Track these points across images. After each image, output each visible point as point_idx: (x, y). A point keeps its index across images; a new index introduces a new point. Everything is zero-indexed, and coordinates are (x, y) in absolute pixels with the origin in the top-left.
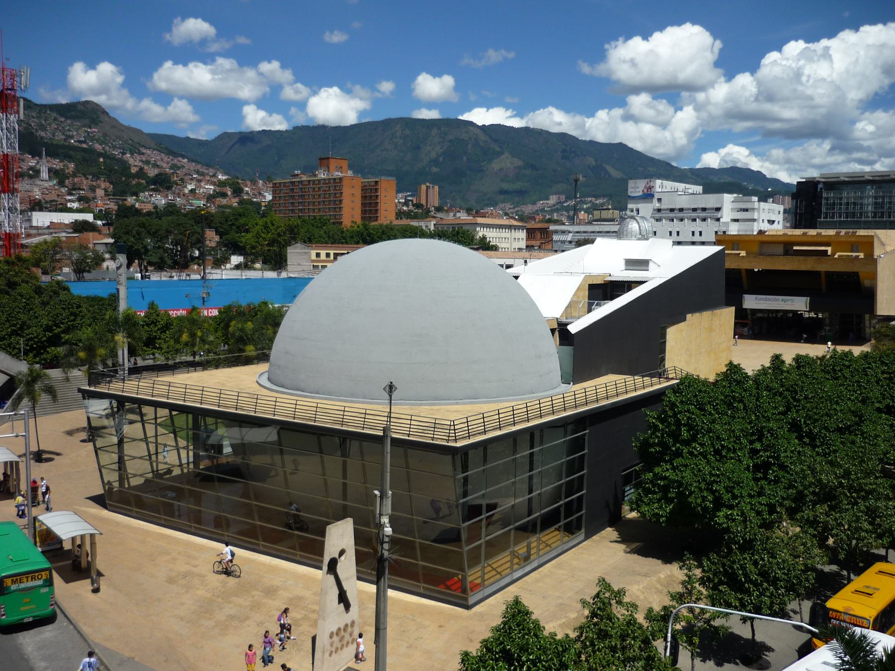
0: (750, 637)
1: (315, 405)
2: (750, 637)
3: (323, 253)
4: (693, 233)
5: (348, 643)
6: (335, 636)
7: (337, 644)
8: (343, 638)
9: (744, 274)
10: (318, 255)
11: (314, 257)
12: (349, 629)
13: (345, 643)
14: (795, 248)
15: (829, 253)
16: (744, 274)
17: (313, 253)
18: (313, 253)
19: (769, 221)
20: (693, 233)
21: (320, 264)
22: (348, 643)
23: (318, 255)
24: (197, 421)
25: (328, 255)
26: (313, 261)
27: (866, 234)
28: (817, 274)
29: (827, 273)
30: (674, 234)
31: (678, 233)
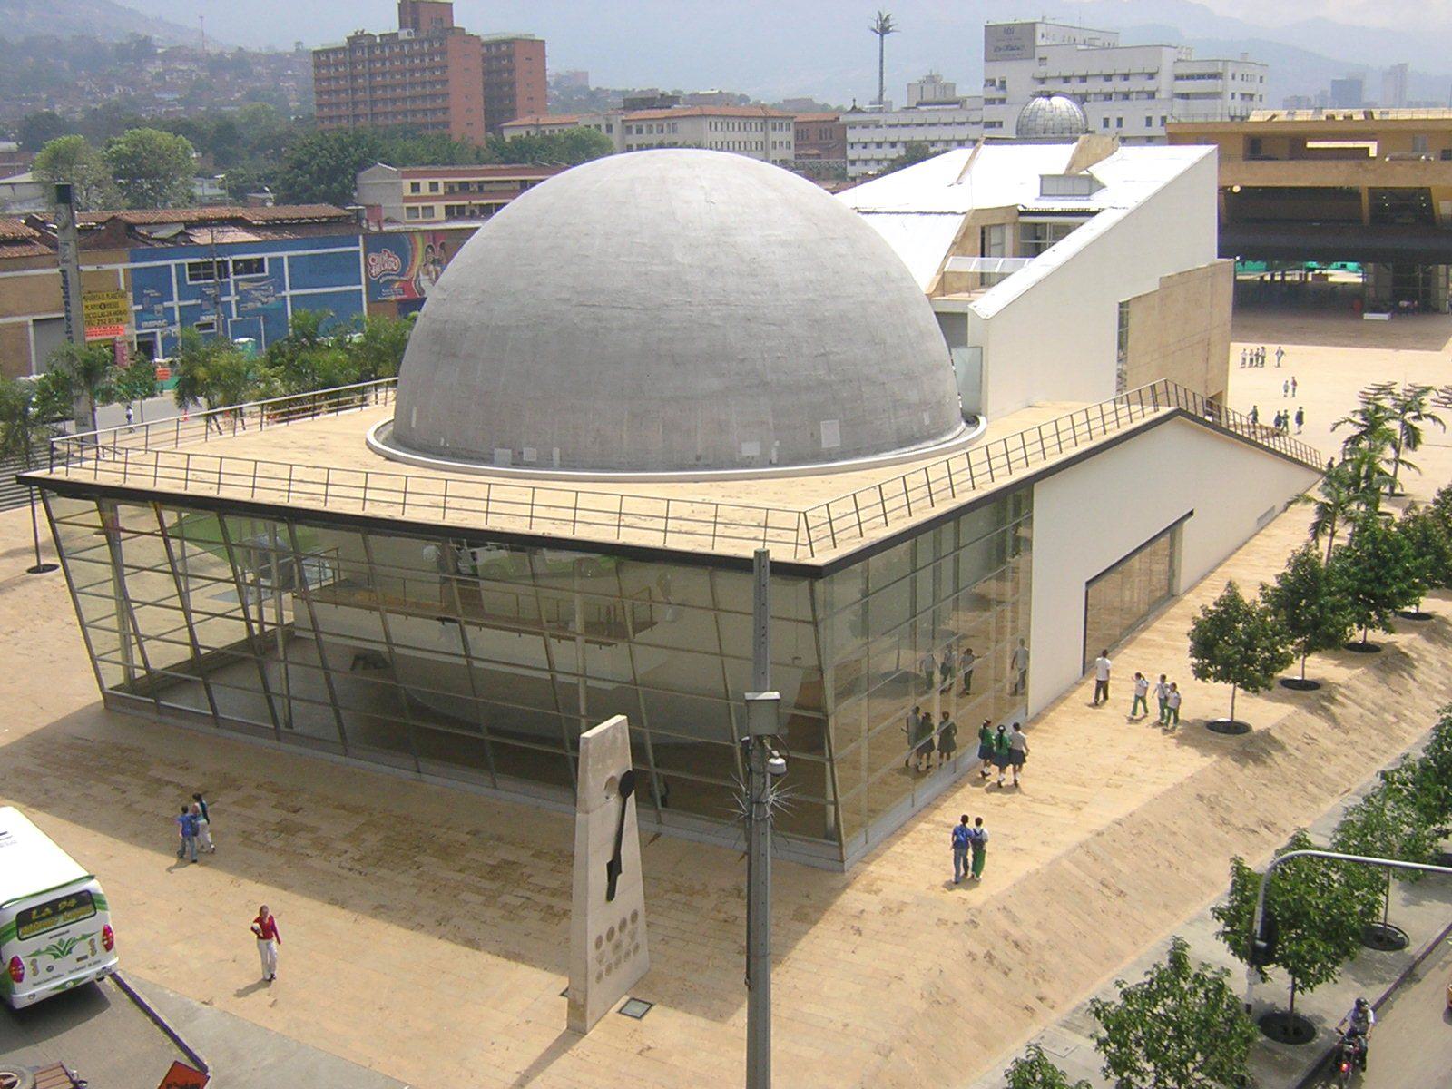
0: (115, 617)
1: (660, 509)
2: (115, 617)
3: (425, 183)
4: (1149, 121)
5: (628, 954)
6: (605, 942)
7: (610, 958)
8: (618, 946)
9: (1365, 199)
10: (416, 187)
11: (408, 192)
12: (629, 926)
13: (622, 953)
14: (1310, 145)
15: (1373, 153)
16: (1365, 199)
17: (407, 183)
18: (407, 183)
19: (1243, 95)
20: (1149, 121)
21: (420, 205)
22: (628, 954)
23: (416, 187)
24: (265, 536)
25: (434, 186)
26: (407, 199)
27: (1408, 117)
28: (1351, 194)
29: (1373, 192)
30: (1113, 123)
31: (1120, 121)
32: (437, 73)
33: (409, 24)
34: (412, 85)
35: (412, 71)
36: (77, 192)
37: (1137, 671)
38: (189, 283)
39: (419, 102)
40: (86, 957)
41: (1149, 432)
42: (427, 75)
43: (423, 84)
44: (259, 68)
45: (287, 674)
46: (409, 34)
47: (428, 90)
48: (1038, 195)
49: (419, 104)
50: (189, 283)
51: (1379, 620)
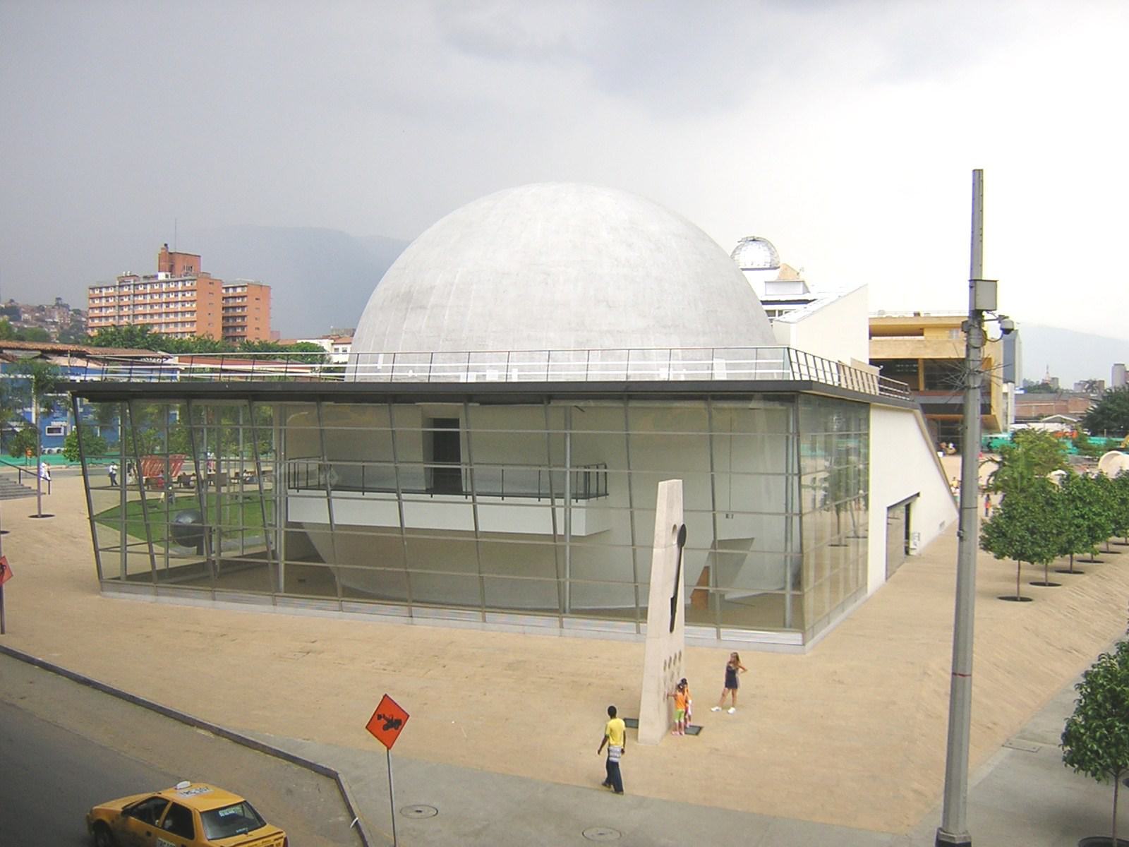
32: (156, 287)
33: (167, 270)
34: (167, 314)
35: (168, 303)
36: (1106, 525)
37: (167, 243)
38: (47, 434)
39: (156, 317)
40: (276, 531)
41: (932, 460)
42: (179, 306)
43: (176, 313)
44: (26, 315)
45: (527, 465)
46: (167, 276)
47: (179, 318)
48: (998, 282)
49: (164, 319)
50: (47, 434)
51: (1092, 553)
